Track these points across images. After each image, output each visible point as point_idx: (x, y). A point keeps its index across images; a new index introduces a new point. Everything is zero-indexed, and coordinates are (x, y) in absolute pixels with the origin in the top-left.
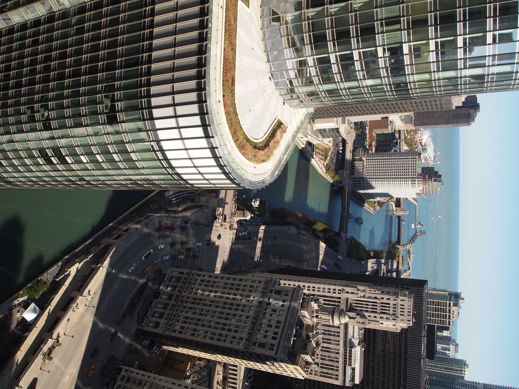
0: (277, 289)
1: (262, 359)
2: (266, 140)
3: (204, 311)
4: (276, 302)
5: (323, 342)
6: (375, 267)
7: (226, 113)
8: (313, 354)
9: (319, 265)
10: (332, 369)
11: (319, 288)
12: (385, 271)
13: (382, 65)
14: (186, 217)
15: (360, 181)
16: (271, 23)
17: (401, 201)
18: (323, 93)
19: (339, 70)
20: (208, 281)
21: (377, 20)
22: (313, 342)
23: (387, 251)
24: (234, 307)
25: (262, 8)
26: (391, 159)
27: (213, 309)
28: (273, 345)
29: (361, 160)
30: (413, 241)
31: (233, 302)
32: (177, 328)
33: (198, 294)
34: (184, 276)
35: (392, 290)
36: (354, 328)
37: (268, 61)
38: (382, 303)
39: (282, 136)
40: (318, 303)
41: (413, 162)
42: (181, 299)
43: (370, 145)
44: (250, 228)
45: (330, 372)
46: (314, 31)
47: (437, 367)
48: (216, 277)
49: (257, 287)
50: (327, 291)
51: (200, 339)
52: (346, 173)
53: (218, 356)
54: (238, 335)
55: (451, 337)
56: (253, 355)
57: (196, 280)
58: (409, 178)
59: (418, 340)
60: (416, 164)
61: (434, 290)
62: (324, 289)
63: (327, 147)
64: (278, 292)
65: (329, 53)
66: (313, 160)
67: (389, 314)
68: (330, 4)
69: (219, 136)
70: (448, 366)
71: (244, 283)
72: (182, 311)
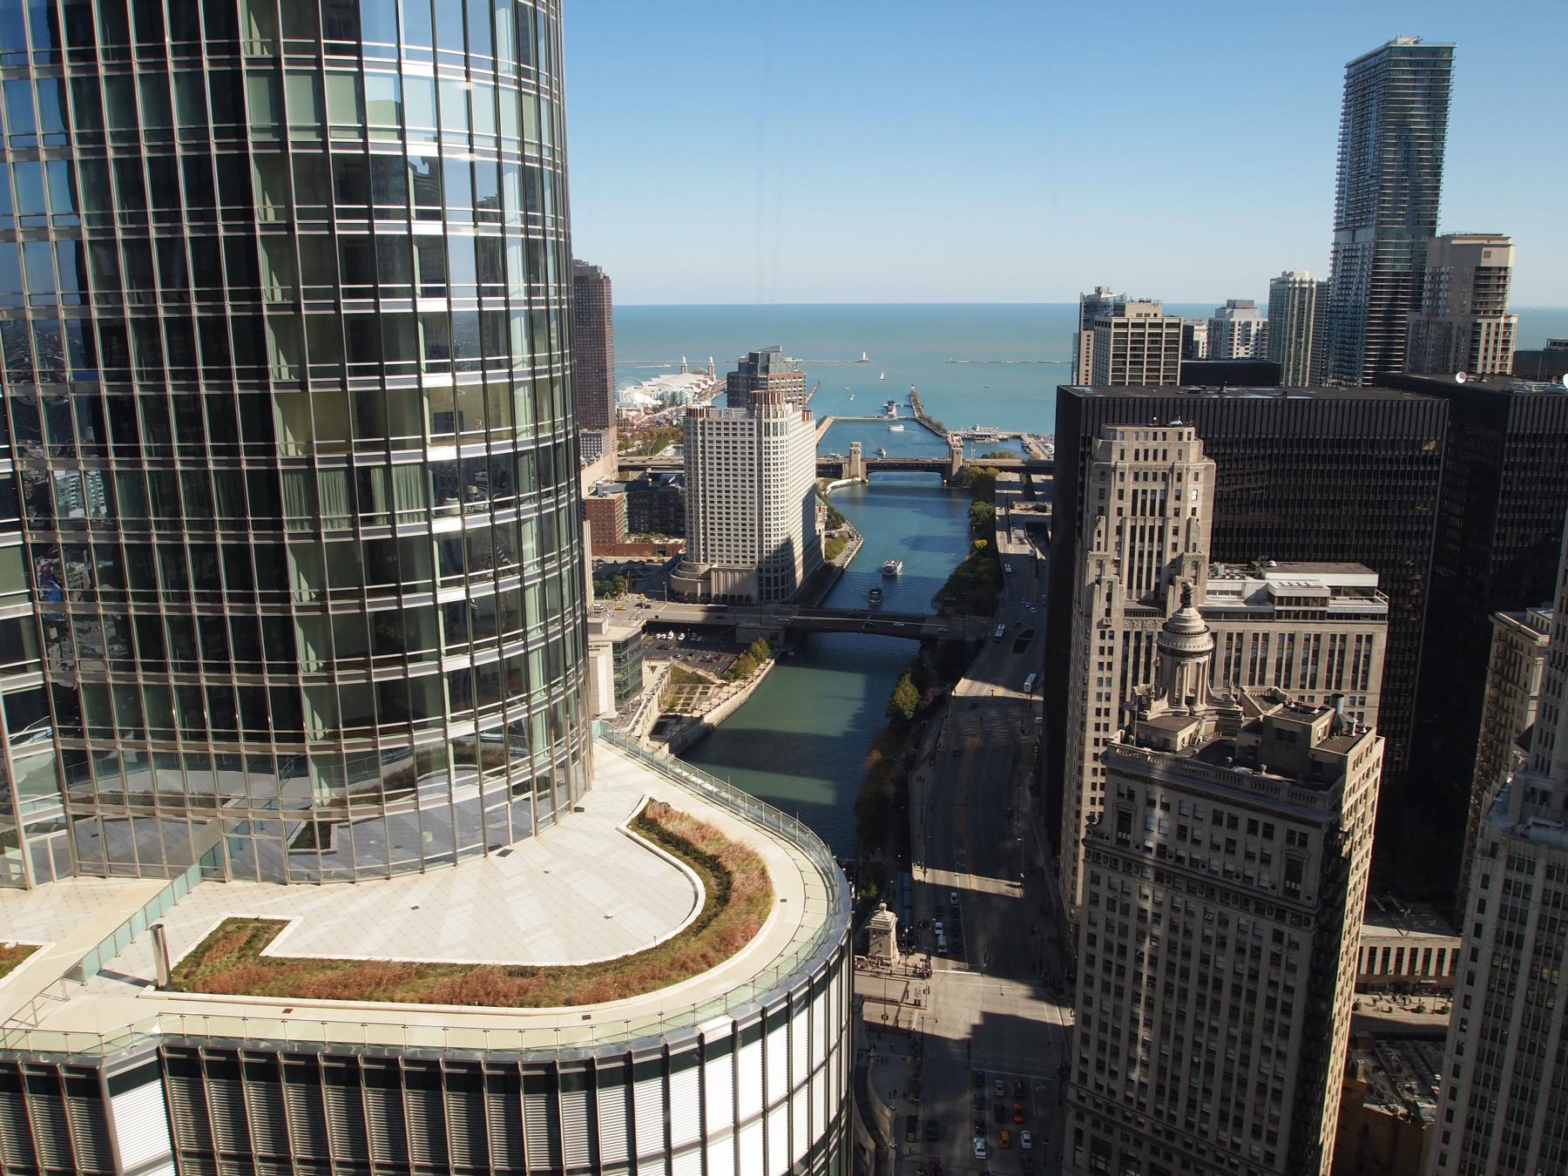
0: (1115, 825)
1: (1337, 868)
2: (698, 867)
3: (1196, 1060)
4: (1157, 829)
5: (1262, 681)
6: (1021, 533)
7: (622, 996)
8: (1306, 712)
9: (1024, 696)
10: (1342, 653)
11: (1099, 696)
12: (1030, 506)
13: (484, 520)
14: (896, 1123)
15: (768, 579)
16: (334, 852)
17: (824, 461)
18: (555, 691)
19: (490, 645)
20: (1102, 1046)
21: (355, 534)
22: (1270, 713)
23: (970, 501)
24: (1178, 960)
25: (289, 880)
26: (704, 491)
27: (1188, 1031)
28: (1291, 834)
29: (706, 577)
30: (939, 427)
31: (1162, 965)
32: (1258, 1149)
33: (1143, 1079)
34: (1086, 1126)
35: (1093, 485)
36: (1214, 592)
37: (452, 859)
38: (1134, 513)
39: (682, 817)
40: (1149, 700)
41: (715, 432)
42: (1162, 1139)
43: (662, 550)
44: (923, 911)
45: (1349, 659)
46: (373, 717)
47: (1297, 357)
48: (1085, 1020)
49: (1110, 887)
50: (1106, 674)
51: (1289, 1071)
52: (744, 622)
53: (1335, 1010)
54: (1268, 947)
55: (1210, 321)
56: (1326, 897)
57: (1099, 1087)
58: (760, 442)
59: (1232, 412)
60: (719, 423)
61: (1076, 367)
62: (1100, 680)
63: (668, 676)
64: (1124, 821)
65: (441, 674)
66: (707, 719)
67: (1165, 492)
68: (296, 672)
69: (699, 1017)
70: (1292, 326)
71: (1100, 931)
72: (1204, 1133)
